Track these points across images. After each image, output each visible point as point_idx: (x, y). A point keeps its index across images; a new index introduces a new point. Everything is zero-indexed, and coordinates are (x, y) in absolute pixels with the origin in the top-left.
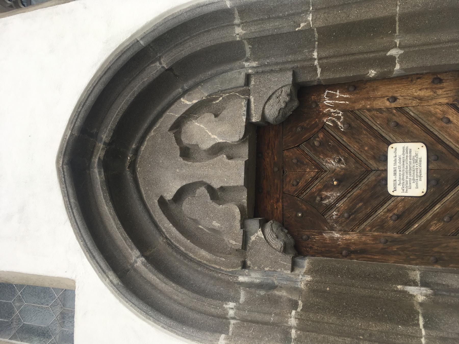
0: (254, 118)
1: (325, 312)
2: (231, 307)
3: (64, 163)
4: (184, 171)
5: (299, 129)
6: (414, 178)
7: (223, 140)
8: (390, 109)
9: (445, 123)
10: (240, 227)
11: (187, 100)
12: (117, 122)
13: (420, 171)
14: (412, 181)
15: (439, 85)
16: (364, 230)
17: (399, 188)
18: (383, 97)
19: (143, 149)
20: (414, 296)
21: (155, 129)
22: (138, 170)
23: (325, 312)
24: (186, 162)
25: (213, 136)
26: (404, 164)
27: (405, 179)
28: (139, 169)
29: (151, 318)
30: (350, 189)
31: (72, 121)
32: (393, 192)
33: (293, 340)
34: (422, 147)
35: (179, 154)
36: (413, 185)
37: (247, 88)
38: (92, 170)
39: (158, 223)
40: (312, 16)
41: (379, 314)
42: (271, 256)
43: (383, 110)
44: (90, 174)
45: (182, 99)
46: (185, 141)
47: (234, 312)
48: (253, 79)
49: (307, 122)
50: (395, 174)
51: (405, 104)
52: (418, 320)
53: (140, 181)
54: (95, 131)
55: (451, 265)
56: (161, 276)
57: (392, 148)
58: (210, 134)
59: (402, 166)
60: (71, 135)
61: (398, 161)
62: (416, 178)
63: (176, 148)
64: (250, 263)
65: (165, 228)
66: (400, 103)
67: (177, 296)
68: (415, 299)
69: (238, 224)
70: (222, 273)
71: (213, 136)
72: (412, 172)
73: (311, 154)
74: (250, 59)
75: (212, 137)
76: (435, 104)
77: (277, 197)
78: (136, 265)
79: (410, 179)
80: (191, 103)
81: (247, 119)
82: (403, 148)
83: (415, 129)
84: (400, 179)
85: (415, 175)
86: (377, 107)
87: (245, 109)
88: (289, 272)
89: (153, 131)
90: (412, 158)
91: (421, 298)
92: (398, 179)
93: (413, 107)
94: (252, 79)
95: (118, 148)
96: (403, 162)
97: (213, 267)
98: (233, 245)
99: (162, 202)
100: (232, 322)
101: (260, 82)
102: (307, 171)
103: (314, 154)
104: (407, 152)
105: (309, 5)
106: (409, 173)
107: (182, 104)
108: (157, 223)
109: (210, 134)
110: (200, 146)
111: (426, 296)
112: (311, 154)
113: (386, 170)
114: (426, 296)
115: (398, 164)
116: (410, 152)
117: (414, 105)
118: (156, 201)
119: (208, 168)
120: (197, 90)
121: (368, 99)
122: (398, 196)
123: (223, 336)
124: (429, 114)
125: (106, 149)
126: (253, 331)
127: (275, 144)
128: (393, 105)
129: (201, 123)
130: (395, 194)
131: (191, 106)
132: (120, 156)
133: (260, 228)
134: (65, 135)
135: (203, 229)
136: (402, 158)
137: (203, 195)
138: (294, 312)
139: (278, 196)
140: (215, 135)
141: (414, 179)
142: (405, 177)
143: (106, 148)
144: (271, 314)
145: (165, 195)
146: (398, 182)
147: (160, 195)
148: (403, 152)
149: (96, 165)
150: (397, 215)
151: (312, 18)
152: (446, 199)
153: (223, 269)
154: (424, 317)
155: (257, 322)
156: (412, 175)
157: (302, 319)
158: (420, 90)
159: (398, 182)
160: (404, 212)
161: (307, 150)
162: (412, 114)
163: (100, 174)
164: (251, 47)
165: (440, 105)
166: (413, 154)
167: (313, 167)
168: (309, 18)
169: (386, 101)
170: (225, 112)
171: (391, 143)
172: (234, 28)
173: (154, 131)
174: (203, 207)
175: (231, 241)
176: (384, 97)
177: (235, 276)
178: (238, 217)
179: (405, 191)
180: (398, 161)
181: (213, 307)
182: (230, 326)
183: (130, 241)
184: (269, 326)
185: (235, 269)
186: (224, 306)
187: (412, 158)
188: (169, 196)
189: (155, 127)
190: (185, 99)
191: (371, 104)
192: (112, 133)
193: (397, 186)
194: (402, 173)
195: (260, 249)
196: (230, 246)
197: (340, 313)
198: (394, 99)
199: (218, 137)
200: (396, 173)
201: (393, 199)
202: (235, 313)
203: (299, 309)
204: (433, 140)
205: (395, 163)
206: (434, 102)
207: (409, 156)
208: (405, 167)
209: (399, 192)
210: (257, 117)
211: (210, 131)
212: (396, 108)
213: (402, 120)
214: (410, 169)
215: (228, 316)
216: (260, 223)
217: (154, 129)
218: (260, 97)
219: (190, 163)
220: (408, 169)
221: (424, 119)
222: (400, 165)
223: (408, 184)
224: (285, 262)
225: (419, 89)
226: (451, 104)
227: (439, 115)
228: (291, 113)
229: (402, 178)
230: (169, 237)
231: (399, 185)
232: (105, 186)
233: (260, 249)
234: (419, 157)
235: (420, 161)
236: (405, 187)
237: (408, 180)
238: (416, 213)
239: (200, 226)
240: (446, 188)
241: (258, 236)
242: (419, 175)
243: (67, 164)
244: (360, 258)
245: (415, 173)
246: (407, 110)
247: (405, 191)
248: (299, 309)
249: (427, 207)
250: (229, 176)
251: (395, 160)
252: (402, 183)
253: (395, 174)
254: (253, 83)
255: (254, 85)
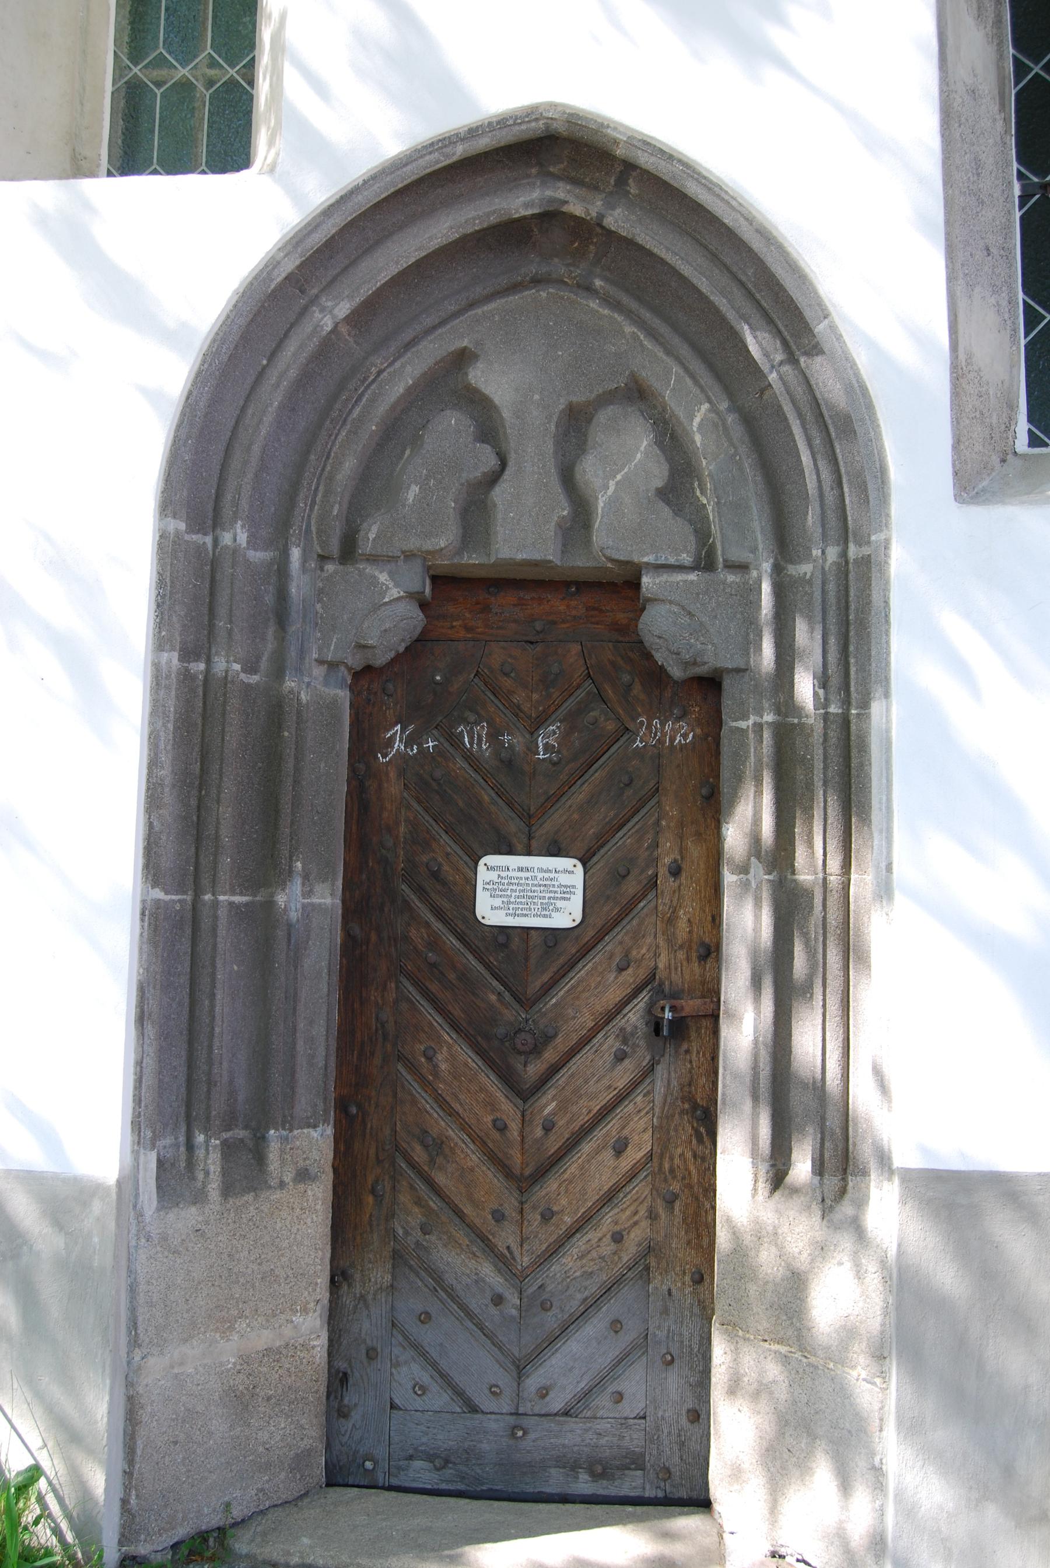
0: (650, 581)
1: (242, 727)
2: (238, 538)
3: (550, 121)
4: (535, 413)
5: (626, 678)
6: (512, 903)
7: (603, 508)
8: (655, 864)
9: (687, 1017)
10: (405, 548)
11: (702, 420)
12: (652, 248)
13: (526, 915)
14: (505, 900)
15: (694, 955)
16: (409, 807)
17: (493, 876)
18: (682, 850)
19: (591, 305)
20: (283, 890)
21: (638, 336)
22: (541, 293)
23: (242, 727)
24: (555, 418)
25: (612, 485)
26: (540, 886)
27: (511, 887)
28: (544, 294)
29: (206, 366)
30: (492, 783)
31: (648, 145)
32: (485, 864)
33: (185, 665)
34: (574, 920)
35: (574, 399)
36: (498, 902)
37: (721, 566)
38: (538, 183)
39: (414, 349)
40: (837, 714)
41: (247, 827)
42: (345, 617)
43: (654, 851)
44: (528, 176)
45: (706, 406)
46: (603, 416)
47: (229, 544)
48: (738, 580)
49: (642, 696)
50: (520, 869)
51: (662, 892)
52: (241, 894)
53: (514, 299)
54: (632, 191)
55: (345, 962)
56: (293, 373)
57: (575, 866)
58: (619, 477)
59: (536, 882)
60: (616, 142)
61: (546, 875)
62: (511, 906)
63: (591, 392)
64: (330, 571)
65: (403, 366)
66: (667, 883)
67: (253, 414)
68: (279, 890)
69: (413, 543)
70: (305, 510)
71: (612, 485)
72: (523, 900)
73: (570, 704)
74: (778, 574)
75: (611, 481)
76: (657, 947)
77: (478, 628)
78: (315, 312)
79: (511, 896)
80: (695, 429)
81: (647, 564)
82: (574, 887)
83: (609, 910)
84: (511, 878)
85: (517, 906)
86: (661, 840)
87: (672, 561)
88: (315, 656)
89: (636, 330)
90: (552, 901)
91: (281, 899)
92: (511, 874)
93: (656, 907)
94: (739, 576)
95: (595, 240)
96: (545, 885)
97: (317, 489)
98: (367, 533)
99: (462, 359)
100: (209, 540)
101: (731, 595)
102: (534, 695)
103: (570, 710)
104: (564, 893)
105: (861, 708)
106: (522, 894)
107: (696, 405)
108: (413, 346)
109: (619, 477)
110: (593, 453)
111: (285, 910)
112: (570, 704)
113: (529, 853)
114: (285, 910)
115: (540, 875)
116: (564, 899)
117: (660, 908)
118: (465, 343)
119: (541, 474)
120: (726, 445)
121: (681, 825)
122: (476, 874)
123: (182, 526)
124: (637, 936)
125: (588, 218)
126: (195, 586)
127: (597, 624)
128: (663, 871)
129: (646, 454)
130: (481, 868)
131: (689, 428)
132: (576, 244)
133: (405, 592)
134: (617, 126)
135: (401, 458)
136: (553, 883)
137: (478, 460)
138: (237, 667)
139: (480, 630)
140: (616, 490)
141: (509, 903)
142: (514, 887)
143: (591, 219)
144: (231, 622)
145: (480, 365)
146: (504, 874)
147: (479, 353)
148: (566, 886)
149: (549, 193)
150: (439, 870)
151: (833, 714)
152: (470, 957)
153: (315, 512)
154: (247, 904)
155: (212, 594)
156: (518, 900)
157: (226, 684)
158: (689, 920)
159: (504, 874)
160: (444, 883)
161: (581, 694)
162: (642, 904)
163: (526, 205)
164: (808, 577)
165: (655, 955)
166: (560, 904)
167: (541, 708)
168: (833, 706)
169: (672, 856)
170: (666, 511)
171: (584, 865)
172: (838, 545)
173: (634, 333)
174: (449, 462)
175: (375, 529)
176: (681, 853)
177: (300, 540)
178: (429, 545)
179: (487, 886)
180: (546, 875)
181: (234, 497)
182: (200, 536)
183: (368, 290)
184: (206, 618)
185: (315, 539)
186: (239, 522)
187: (552, 901)
188: (478, 376)
189: (644, 337)
190: (705, 414)
191: (669, 827)
192: (625, 234)
193: (496, 873)
194: (523, 881)
195: (360, 592)
196: (365, 525)
197: (243, 756)
198: (676, 872)
199: (610, 497)
200: (522, 870)
201: (471, 864)
202: (227, 547)
203: (243, 676)
204: (586, 939)
205: (541, 870)
206: (662, 943)
207: (556, 895)
208: (533, 889)
209: (483, 875)
210: (652, 587)
211: (626, 478)
212: (657, 875)
213: (631, 887)
214: (532, 897)
215: (218, 531)
216: (418, 593)
217: (639, 334)
218: (698, 594)
219: (553, 427)
220: (529, 894)
221: (628, 927)
222: (538, 879)
223: (500, 893)
224: (336, 648)
225: (692, 920)
226: (654, 975)
227: (634, 953)
228: (660, 663)
229: (513, 881)
230: (382, 376)
231: (499, 876)
232: (498, 220)
233: (360, 592)
234: (553, 914)
235: (545, 916)
236: (495, 887)
237: (509, 893)
238: (445, 904)
239: (408, 452)
240: (492, 959)
241: (388, 588)
242: (517, 912)
243: (547, 126)
244: (351, 797)
245: (521, 906)
246: (650, 896)
247: (487, 886)
248: (243, 676)
249: (456, 925)
250: (518, 524)
251: (549, 871)
252: (503, 881)
253: (520, 869)
254: (731, 578)
255: (724, 583)
